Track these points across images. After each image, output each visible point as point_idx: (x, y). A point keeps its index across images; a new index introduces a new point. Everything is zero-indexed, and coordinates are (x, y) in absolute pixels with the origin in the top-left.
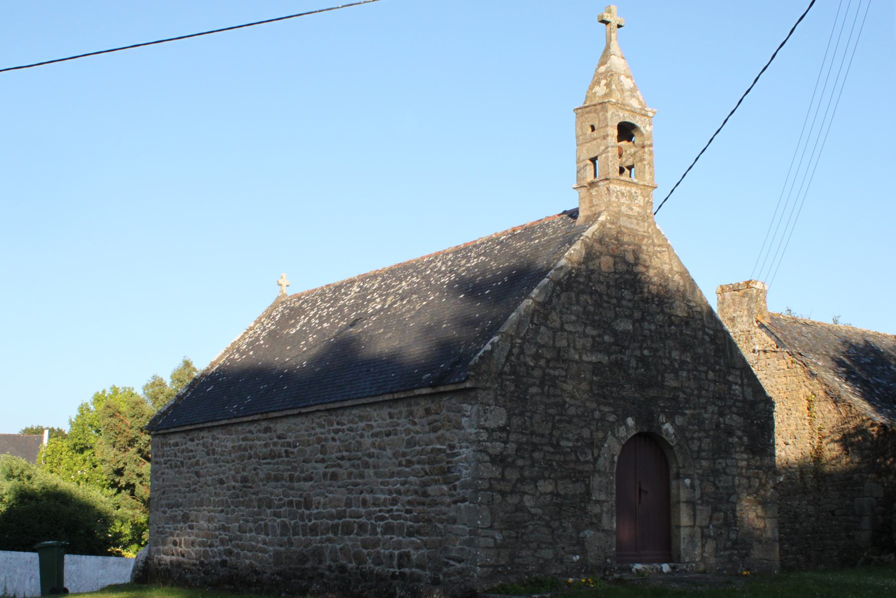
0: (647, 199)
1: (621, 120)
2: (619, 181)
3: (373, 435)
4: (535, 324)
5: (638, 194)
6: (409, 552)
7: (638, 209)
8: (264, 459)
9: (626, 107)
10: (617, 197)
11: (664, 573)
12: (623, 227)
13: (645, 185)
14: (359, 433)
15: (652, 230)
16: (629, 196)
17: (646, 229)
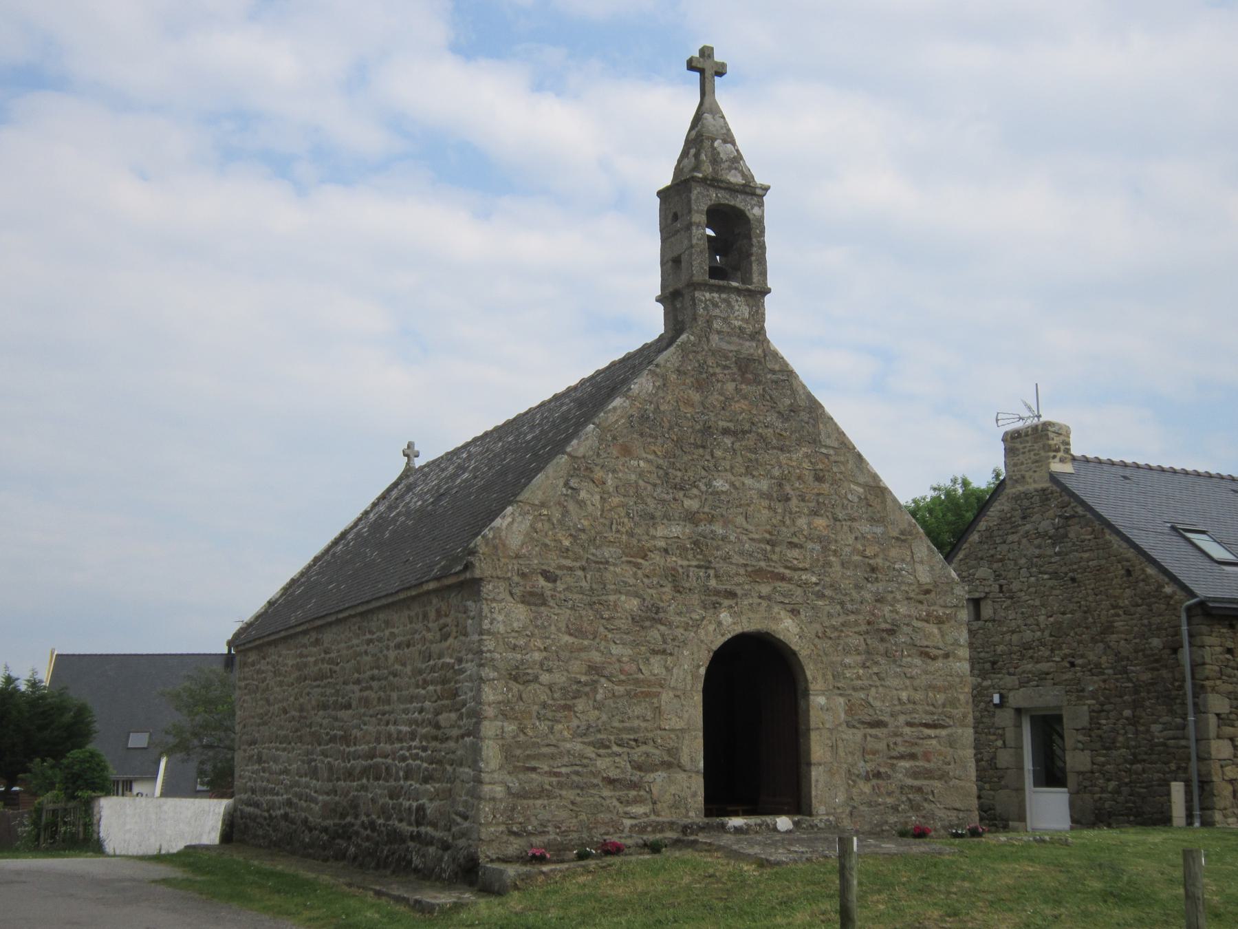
3: (398, 646)
4: (572, 488)
6: (424, 804)
8: (316, 680)
9: (720, 184)
10: (706, 308)
11: (779, 831)
14: (385, 644)
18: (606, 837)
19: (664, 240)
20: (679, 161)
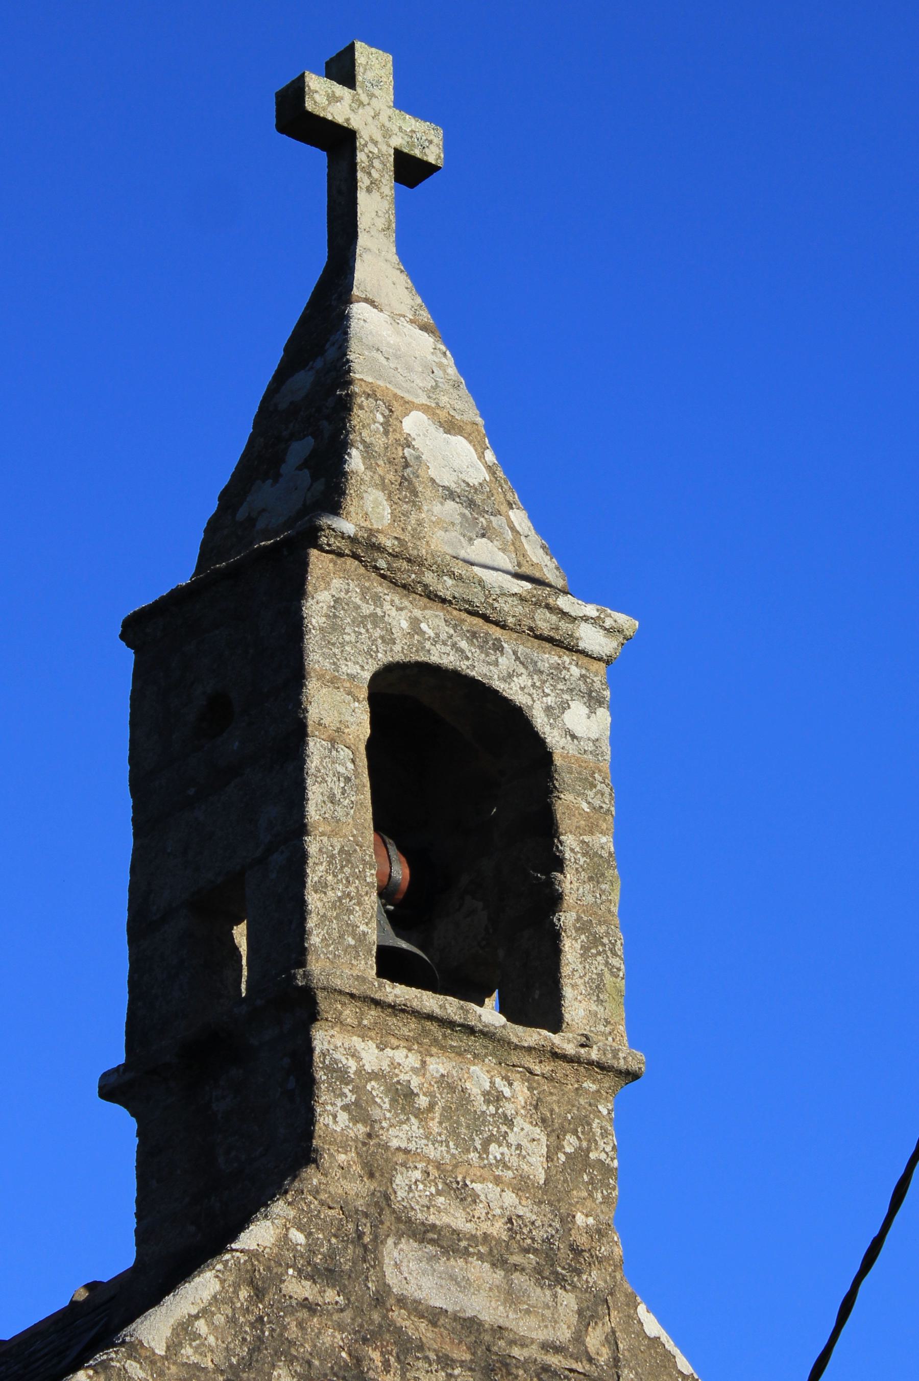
0: (570, 1144)
1: (398, 653)
2: (373, 1014)
5: (509, 1108)
7: (510, 1198)
9: (429, 578)
12: (401, 1301)
13: (557, 1055)
15: (612, 1340)
16: (447, 1115)
17: (564, 1334)
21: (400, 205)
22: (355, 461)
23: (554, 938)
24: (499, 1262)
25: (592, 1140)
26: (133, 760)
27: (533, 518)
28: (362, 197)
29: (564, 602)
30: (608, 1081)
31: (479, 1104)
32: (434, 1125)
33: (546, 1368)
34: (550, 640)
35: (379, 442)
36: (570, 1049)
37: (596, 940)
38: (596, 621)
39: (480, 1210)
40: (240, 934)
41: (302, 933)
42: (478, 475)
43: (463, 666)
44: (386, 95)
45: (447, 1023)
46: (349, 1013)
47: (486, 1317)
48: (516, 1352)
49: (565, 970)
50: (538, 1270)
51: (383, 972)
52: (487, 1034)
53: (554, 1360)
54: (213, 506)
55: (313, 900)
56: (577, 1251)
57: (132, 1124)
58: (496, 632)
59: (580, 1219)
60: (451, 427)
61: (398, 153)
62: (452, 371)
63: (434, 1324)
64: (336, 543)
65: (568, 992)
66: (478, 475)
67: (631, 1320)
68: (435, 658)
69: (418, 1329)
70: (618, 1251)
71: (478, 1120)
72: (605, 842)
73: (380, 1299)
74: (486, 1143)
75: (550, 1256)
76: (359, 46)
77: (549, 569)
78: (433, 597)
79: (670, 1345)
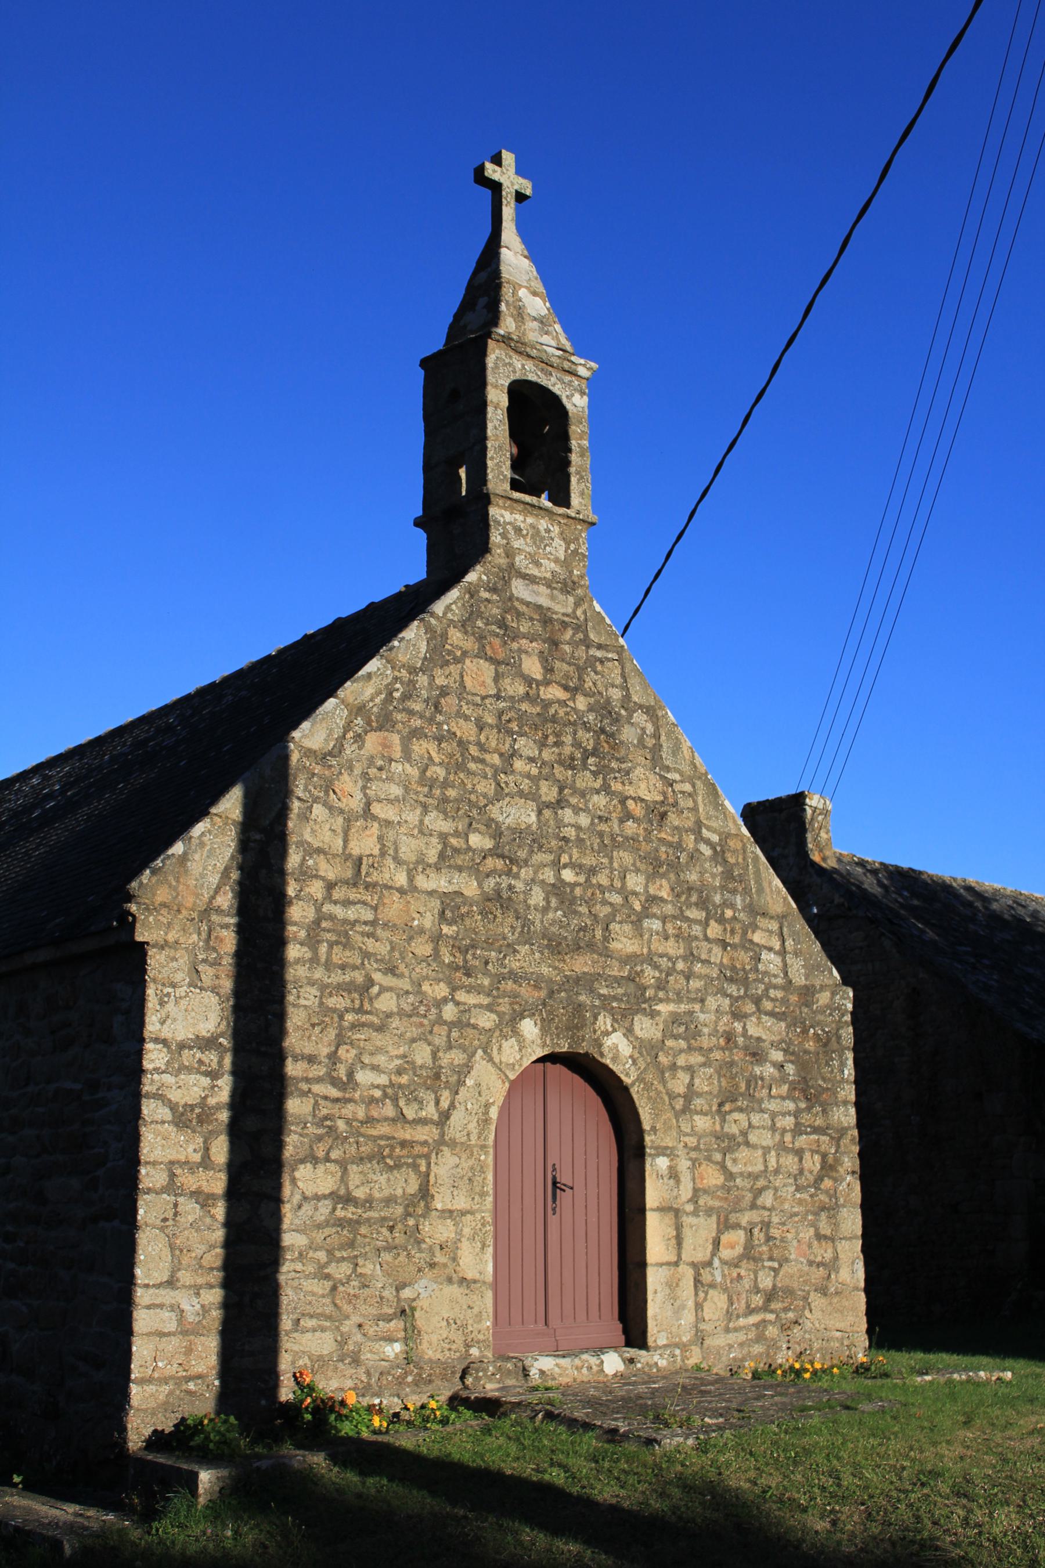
0: (572, 547)
1: (518, 376)
5: (552, 535)
7: (553, 565)
9: (528, 350)
12: (518, 599)
13: (569, 517)
15: (585, 613)
16: (532, 537)
17: (570, 610)
18: (906, 1533)
19: (428, 433)
20: (457, 317)
21: (517, 210)
22: (503, 307)
23: (568, 477)
24: (549, 586)
25: (579, 546)
26: (424, 409)
27: (562, 327)
28: (504, 208)
29: (573, 358)
30: (585, 526)
31: (543, 533)
32: (528, 540)
33: (564, 622)
34: (568, 372)
35: (511, 300)
36: (573, 515)
37: (582, 477)
38: (584, 365)
39: (543, 569)
40: (462, 473)
41: (485, 474)
42: (544, 312)
43: (539, 381)
44: (512, 170)
45: (533, 506)
46: (501, 502)
47: (544, 605)
48: (554, 616)
49: (572, 488)
50: (561, 589)
51: (512, 488)
52: (546, 510)
53: (566, 619)
54: (450, 320)
55: (489, 463)
56: (574, 583)
57: (425, 535)
58: (550, 369)
59: (575, 572)
60: (535, 294)
61: (517, 191)
62: (535, 273)
63: (528, 606)
64: (497, 337)
65: (572, 495)
66: (544, 312)
67: (591, 606)
68: (530, 378)
69: (523, 608)
70: (587, 583)
71: (542, 539)
72: (585, 443)
73: (511, 598)
74: (545, 547)
75: (565, 584)
76: (503, 151)
77: (568, 346)
78: (529, 356)
79: (604, 614)
